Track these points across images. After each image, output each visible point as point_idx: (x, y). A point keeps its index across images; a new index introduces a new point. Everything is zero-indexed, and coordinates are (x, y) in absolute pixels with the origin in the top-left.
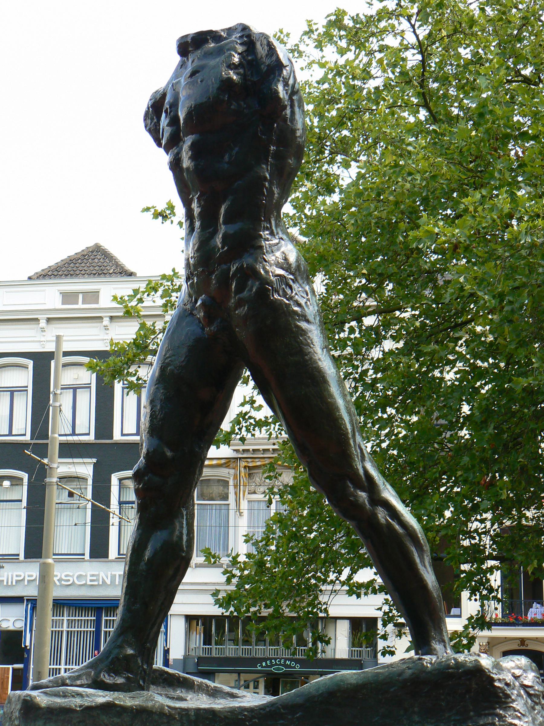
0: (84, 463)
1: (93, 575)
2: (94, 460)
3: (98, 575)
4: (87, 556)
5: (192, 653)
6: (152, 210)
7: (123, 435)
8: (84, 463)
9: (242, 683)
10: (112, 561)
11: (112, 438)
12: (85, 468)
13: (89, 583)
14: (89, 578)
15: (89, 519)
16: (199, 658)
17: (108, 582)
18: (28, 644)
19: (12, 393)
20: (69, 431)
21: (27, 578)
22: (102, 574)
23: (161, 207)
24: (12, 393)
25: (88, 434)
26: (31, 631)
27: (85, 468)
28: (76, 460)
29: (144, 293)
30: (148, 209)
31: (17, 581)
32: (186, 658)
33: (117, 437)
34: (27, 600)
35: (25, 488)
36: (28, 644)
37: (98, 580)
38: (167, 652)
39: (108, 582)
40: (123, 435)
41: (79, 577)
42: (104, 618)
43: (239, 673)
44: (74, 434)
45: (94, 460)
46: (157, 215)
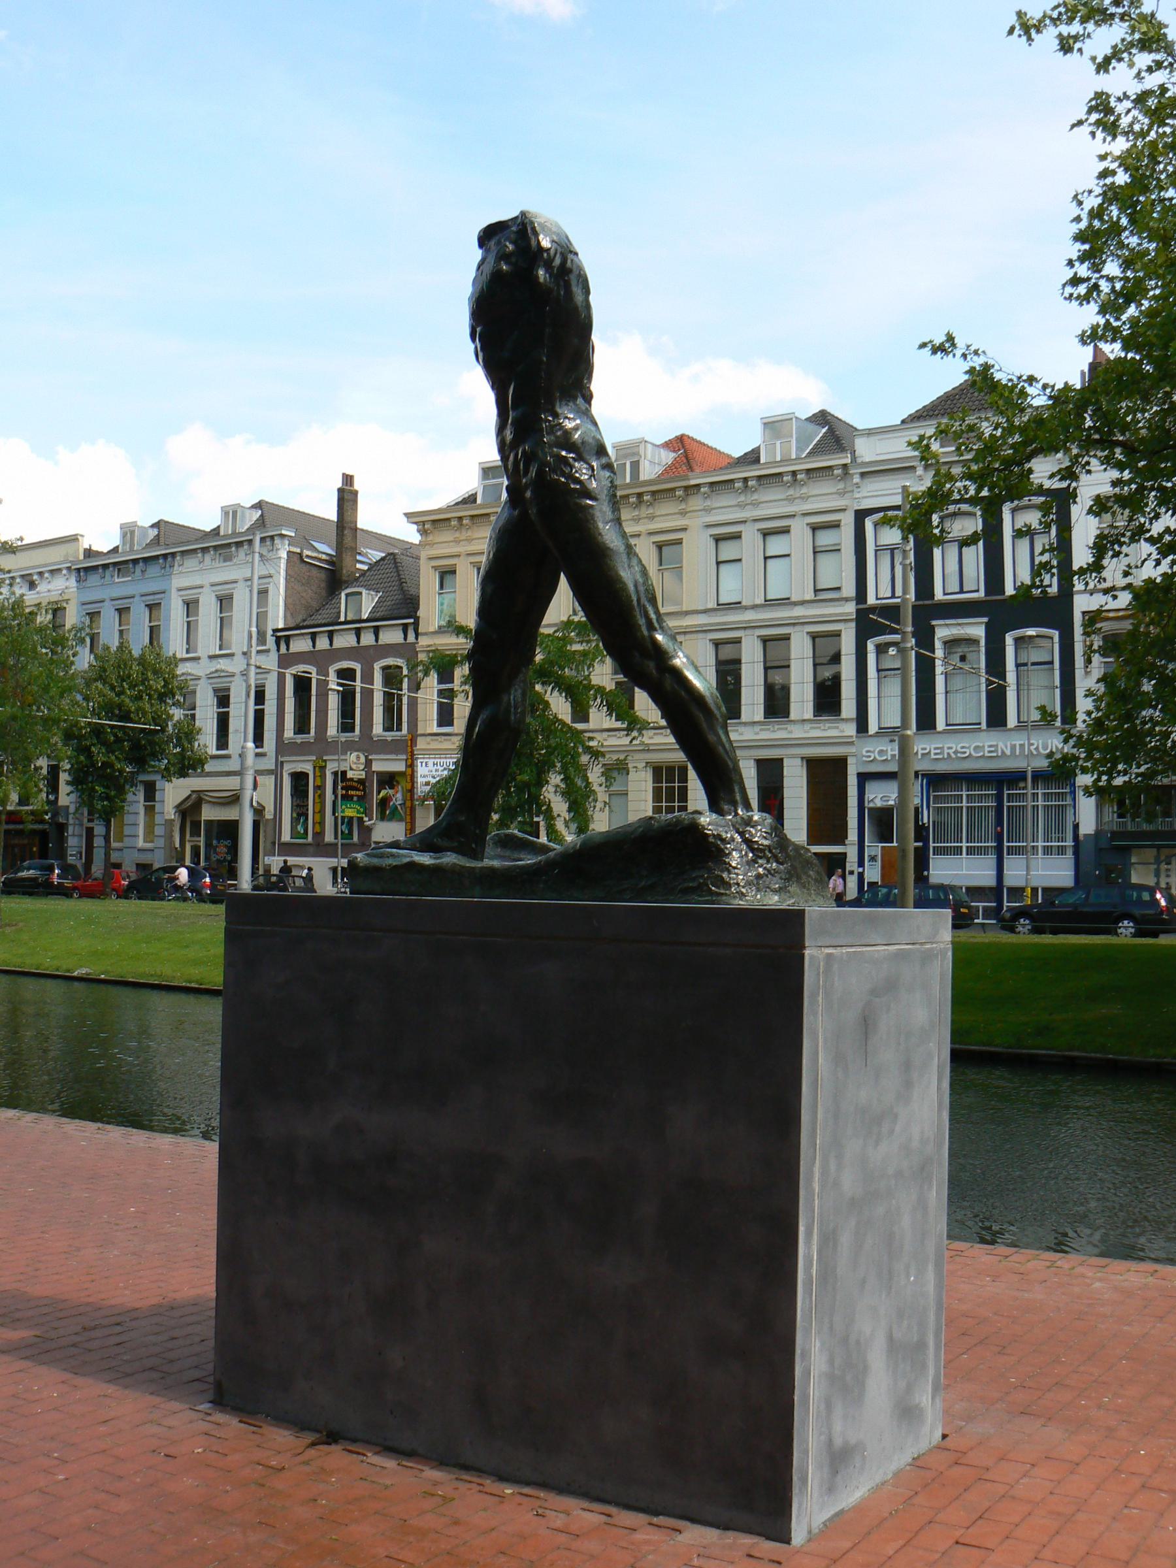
0: (959, 624)
1: (990, 746)
2: (985, 620)
3: (997, 746)
4: (984, 726)
5: (1106, 827)
6: (930, 346)
7: (945, 594)
8: (959, 624)
9: (1163, 858)
10: (1011, 730)
11: (1004, 593)
12: (977, 629)
13: (987, 754)
14: (987, 749)
15: (1057, 682)
16: (1113, 833)
17: (1008, 752)
18: (925, 821)
19: (892, 550)
20: (957, 590)
21: (920, 752)
22: (1001, 745)
23: (939, 339)
24: (892, 550)
25: (977, 591)
26: (928, 807)
27: (977, 629)
28: (960, 621)
29: (930, 437)
30: (923, 346)
31: (923, 755)
32: (1098, 833)
33: (939, 595)
34: (923, 775)
35: (983, 650)
36: (925, 821)
37: (996, 751)
38: (1076, 827)
39: (1008, 752)
40: (945, 594)
41: (976, 748)
42: (1006, 792)
43: (1159, 847)
44: (961, 591)
45: (985, 620)
46: (935, 350)
